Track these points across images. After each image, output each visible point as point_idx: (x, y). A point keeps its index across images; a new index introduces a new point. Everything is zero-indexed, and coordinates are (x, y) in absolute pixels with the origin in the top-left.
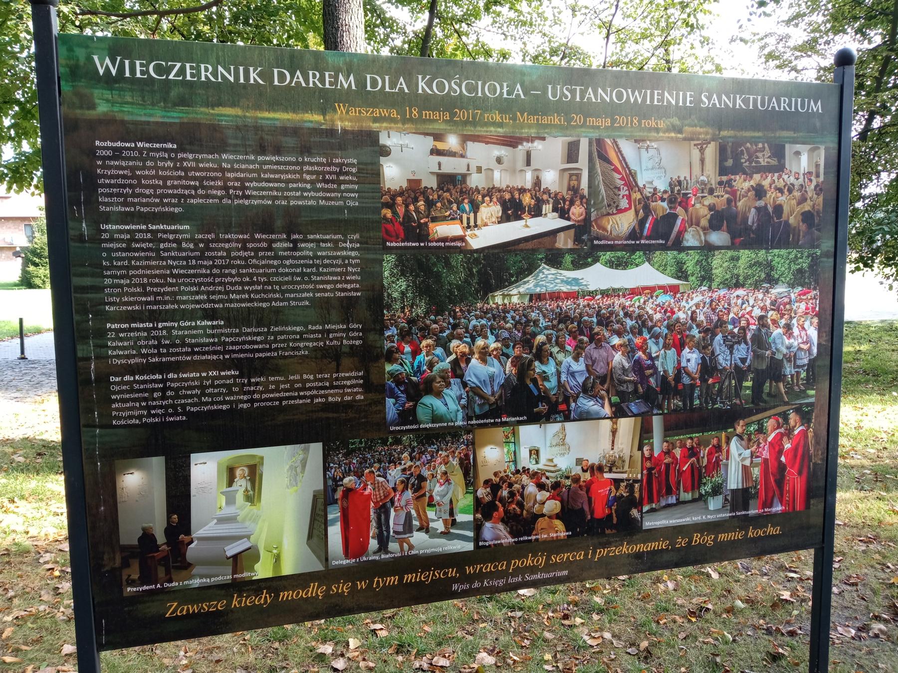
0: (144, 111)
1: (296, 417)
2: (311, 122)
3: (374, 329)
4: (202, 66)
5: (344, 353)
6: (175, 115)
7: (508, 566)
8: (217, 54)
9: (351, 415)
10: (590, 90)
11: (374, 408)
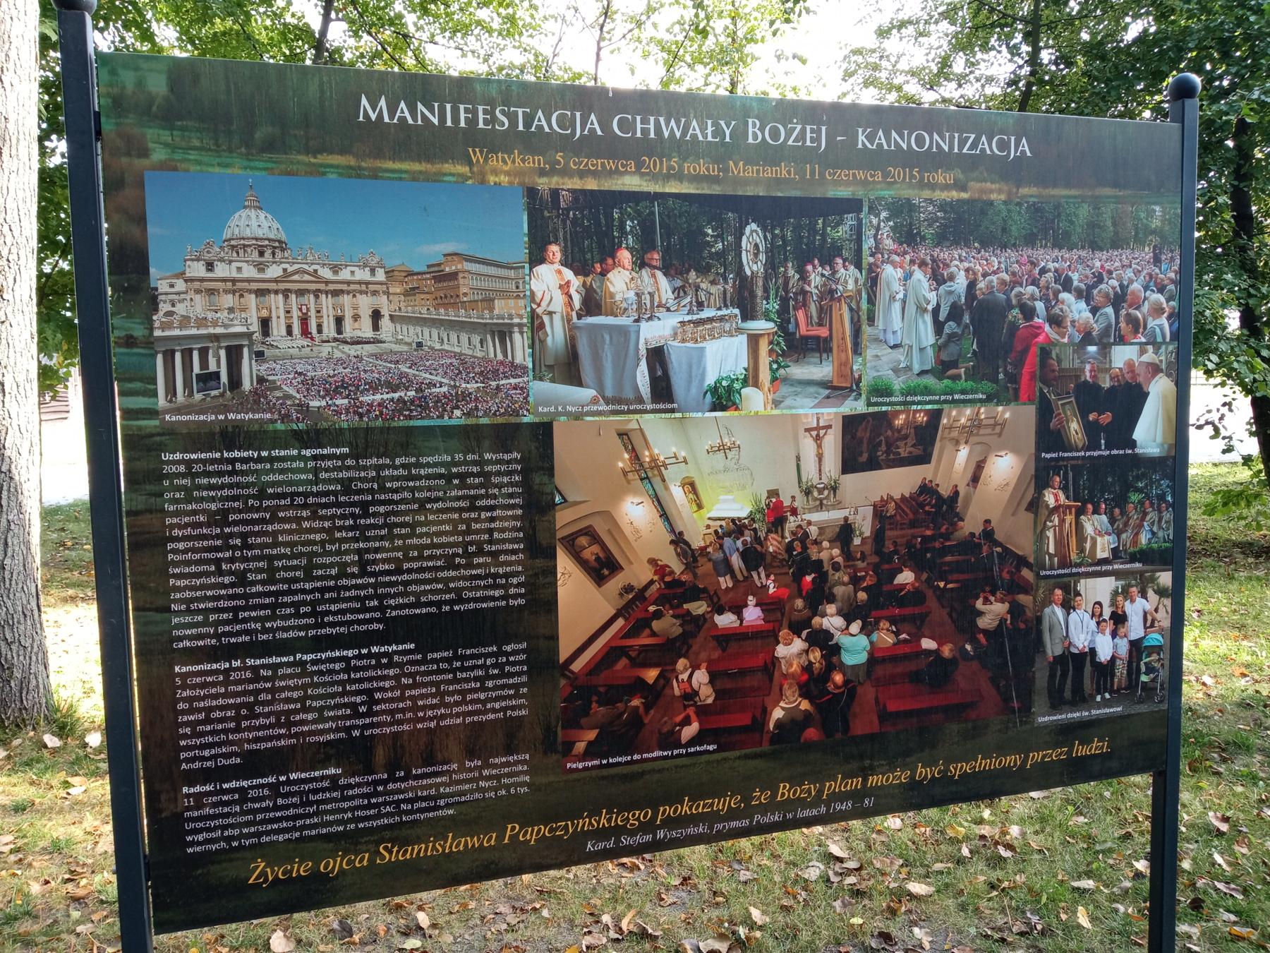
0: (218, 160)
2: (452, 175)
3: (543, 468)
8: (321, 79)
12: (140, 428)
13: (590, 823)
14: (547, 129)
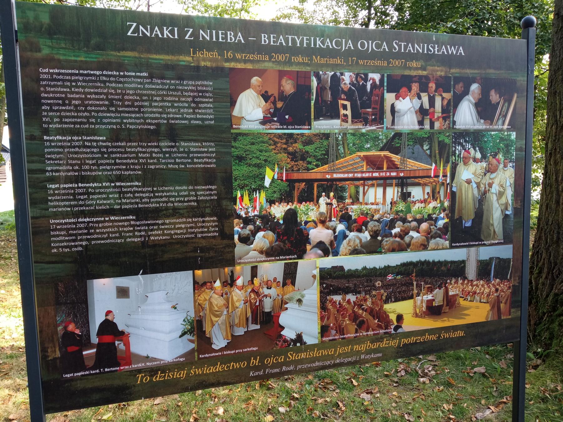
1: (176, 256)
2: (184, 61)
4: (229, 33)
5: (208, 213)
6: (94, 56)
7: (335, 351)
9: (212, 254)
10: (410, 45)
11: (227, 250)
12: (38, 178)
13: (169, 376)
14: (331, 47)
